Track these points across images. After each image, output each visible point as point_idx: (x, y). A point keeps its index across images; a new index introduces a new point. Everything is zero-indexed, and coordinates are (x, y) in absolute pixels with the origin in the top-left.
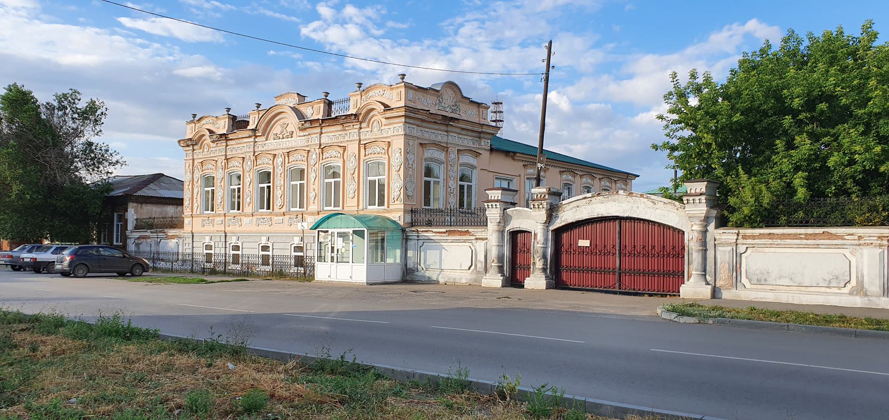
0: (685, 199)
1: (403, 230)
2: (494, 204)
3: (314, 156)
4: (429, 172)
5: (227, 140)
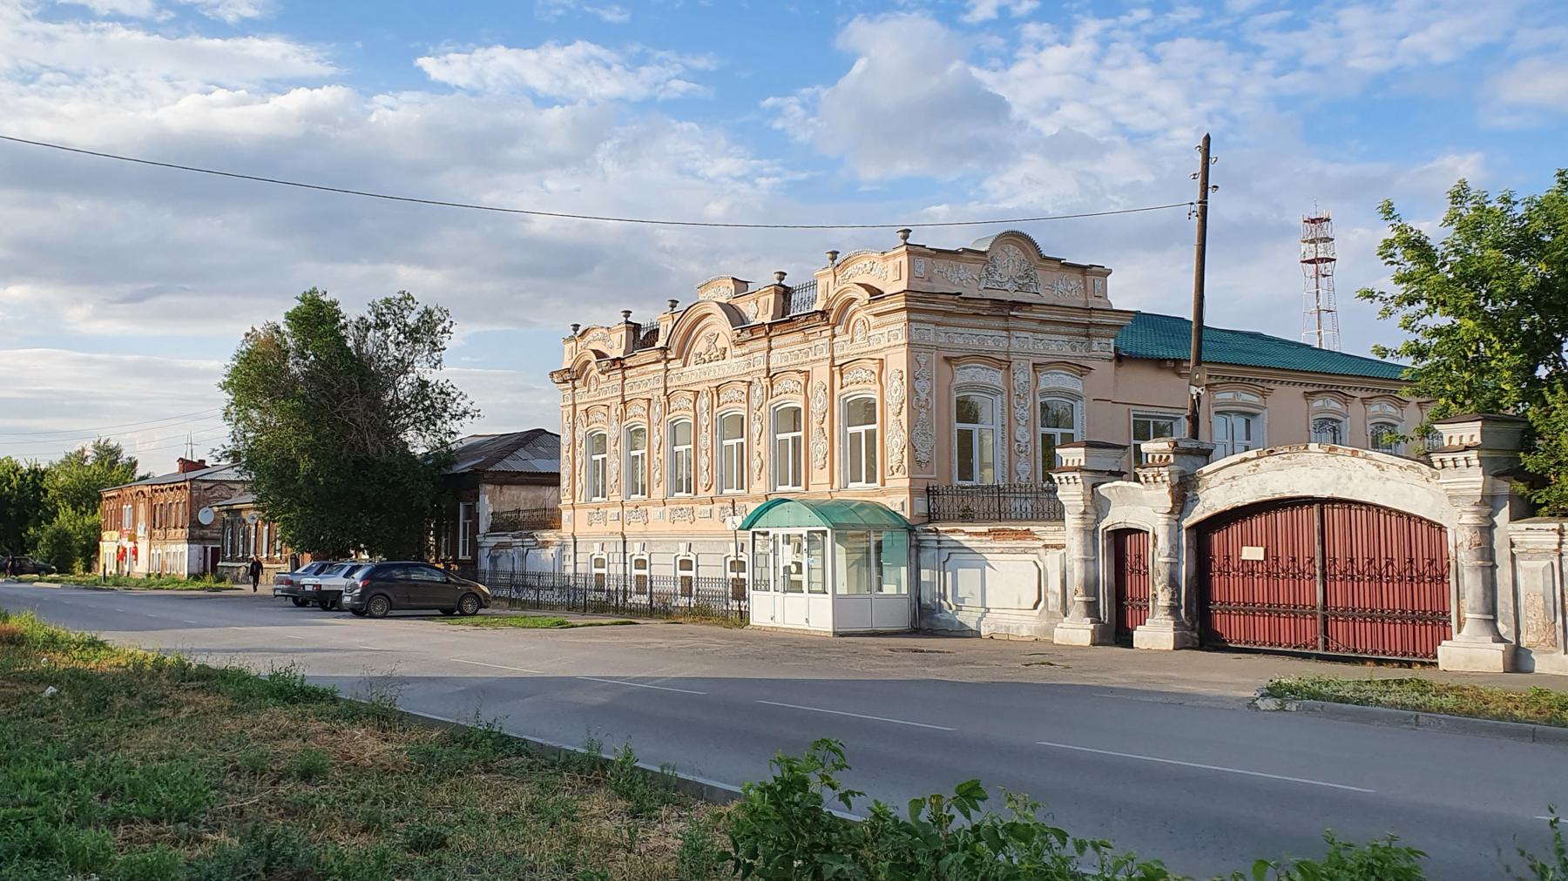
0: (1435, 458)
1: (911, 530)
2: (1070, 475)
3: (758, 392)
4: (967, 412)
5: (624, 368)
